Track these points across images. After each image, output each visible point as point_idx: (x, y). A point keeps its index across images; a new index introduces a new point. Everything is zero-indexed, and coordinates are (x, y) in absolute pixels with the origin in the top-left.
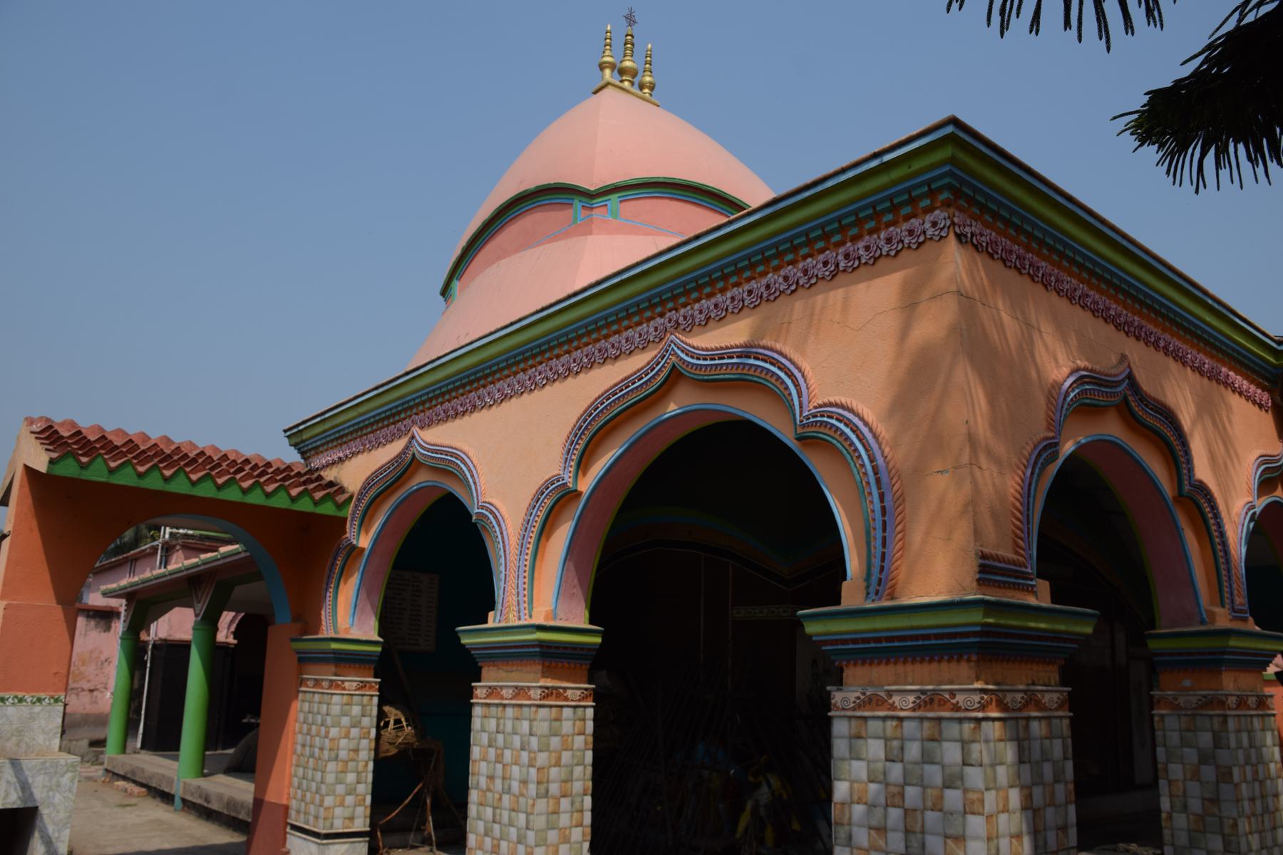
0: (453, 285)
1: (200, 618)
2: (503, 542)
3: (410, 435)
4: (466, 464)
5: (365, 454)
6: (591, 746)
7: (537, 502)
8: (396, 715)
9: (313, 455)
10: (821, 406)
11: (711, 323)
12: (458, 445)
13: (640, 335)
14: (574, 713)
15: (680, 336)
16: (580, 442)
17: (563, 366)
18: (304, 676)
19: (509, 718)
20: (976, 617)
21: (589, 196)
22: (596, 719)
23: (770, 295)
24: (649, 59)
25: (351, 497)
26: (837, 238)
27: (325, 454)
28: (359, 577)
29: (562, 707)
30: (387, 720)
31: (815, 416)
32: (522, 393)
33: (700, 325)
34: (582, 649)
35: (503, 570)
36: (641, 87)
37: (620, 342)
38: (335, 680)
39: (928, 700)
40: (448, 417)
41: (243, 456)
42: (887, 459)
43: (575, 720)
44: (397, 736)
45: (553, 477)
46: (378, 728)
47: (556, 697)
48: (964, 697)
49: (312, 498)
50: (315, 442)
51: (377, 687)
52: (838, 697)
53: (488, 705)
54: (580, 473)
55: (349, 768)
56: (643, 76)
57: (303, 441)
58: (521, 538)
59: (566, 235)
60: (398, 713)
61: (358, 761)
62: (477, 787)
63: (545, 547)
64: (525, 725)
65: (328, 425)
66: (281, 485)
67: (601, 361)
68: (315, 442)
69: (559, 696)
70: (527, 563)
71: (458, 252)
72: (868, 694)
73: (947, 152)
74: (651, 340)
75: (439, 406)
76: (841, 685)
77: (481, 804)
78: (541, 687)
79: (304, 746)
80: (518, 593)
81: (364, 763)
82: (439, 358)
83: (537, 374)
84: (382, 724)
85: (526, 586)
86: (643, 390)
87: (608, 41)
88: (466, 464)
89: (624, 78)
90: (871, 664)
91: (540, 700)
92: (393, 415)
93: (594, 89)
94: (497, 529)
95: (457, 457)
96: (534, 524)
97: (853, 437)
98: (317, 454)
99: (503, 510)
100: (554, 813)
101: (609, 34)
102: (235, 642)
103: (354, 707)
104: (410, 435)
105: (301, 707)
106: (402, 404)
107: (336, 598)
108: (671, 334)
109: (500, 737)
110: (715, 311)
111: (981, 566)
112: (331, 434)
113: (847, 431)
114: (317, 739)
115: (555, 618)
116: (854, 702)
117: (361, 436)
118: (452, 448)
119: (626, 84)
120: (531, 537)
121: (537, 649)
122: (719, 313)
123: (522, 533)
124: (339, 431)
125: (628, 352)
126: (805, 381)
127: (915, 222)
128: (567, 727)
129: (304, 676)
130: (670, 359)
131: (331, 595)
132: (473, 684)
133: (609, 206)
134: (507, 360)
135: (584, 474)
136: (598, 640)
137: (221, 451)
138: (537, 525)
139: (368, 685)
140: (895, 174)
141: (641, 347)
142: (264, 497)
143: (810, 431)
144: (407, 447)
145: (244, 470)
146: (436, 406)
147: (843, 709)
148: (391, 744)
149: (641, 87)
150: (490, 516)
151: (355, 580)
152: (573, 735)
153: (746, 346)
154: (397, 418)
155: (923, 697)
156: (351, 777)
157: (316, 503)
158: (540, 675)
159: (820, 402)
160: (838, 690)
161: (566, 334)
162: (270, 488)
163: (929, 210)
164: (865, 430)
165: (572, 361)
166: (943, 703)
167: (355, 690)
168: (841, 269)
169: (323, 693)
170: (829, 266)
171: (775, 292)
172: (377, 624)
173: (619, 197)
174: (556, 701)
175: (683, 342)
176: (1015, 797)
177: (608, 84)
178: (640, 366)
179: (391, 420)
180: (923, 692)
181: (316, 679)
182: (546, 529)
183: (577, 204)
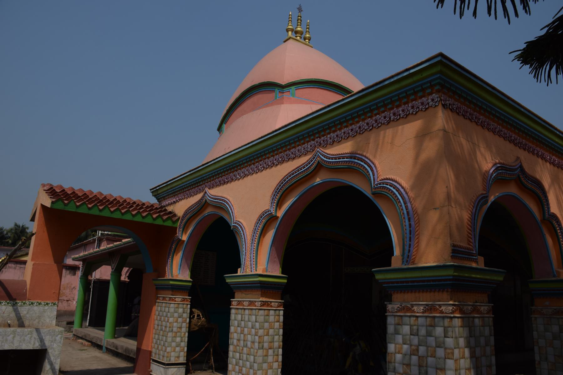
0: (223, 126)
1: (114, 270)
2: (244, 238)
4: (228, 204)
5: (185, 200)
6: (282, 327)
7: (259, 221)
8: (198, 313)
9: (163, 200)
10: (383, 180)
11: (335, 143)
12: (225, 196)
13: (304, 149)
14: (275, 313)
15: (322, 149)
16: (278, 195)
17: (270, 162)
18: (158, 295)
22: (284, 315)
23: (361, 131)
24: (308, 27)
25: (179, 218)
26: (390, 106)
28: (182, 253)
29: (269, 310)
30: (194, 315)
31: (380, 184)
32: (253, 174)
33: (330, 144)
34: (268, 284)
35: (244, 251)
36: (305, 39)
37: (295, 151)
38: (172, 297)
39: (430, 309)
40: (221, 184)
41: (133, 200)
42: (412, 203)
43: (275, 316)
44: (198, 322)
45: (266, 210)
46: (190, 318)
47: (267, 306)
48: (445, 307)
49: (162, 219)
50: (164, 194)
51: (190, 300)
52: (389, 307)
53: (237, 309)
56: (306, 34)
57: (158, 194)
59: (272, 104)
60: (199, 312)
61: (181, 333)
64: (253, 318)
65: (169, 187)
66: (149, 213)
67: (287, 160)
68: (164, 194)
69: (268, 305)
70: (255, 247)
71: (225, 112)
72: (403, 305)
76: (391, 301)
77: (163, 336)
78: (260, 301)
79: (158, 325)
81: (184, 333)
82: (217, 158)
83: (259, 165)
84: (192, 317)
85: (254, 257)
87: (290, 19)
88: (228, 204)
89: (297, 35)
90: (404, 293)
92: (197, 183)
93: (284, 40)
94: (242, 232)
95: (225, 201)
96: (258, 230)
97: (397, 193)
98: (164, 200)
99: (245, 224)
100: (174, 337)
102: (129, 280)
103: (180, 309)
106: (201, 178)
108: (318, 148)
109: (243, 323)
111: (453, 250)
112: (171, 191)
114: (164, 322)
115: (267, 271)
116: (397, 309)
117: (183, 192)
118: (223, 197)
119: (298, 38)
120: (256, 236)
121: (259, 285)
122: (338, 139)
124: (174, 190)
125: (299, 156)
126: (376, 169)
128: (272, 318)
129: (158, 295)
131: (170, 260)
132: (231, 300)
133: (291, 91)
134: (246, 159)
135: (280, 209)
137: (123, 198)
138: (259, 231)
139: (186, 300)
140: (415, 78)
141: (304, 154)
142: (141, 218)
143: (378, 191)
144: (203, 197)
146: (216, 179)
147: (392, 312)
149: (305, 39)
150: (239, 227)
151: (180, 254)
153: (352, 154)
155: (427, 307)
156: (178, 339)
157: (164, 221)
158: (260, 296)
159: (383, 178)
160: (390, 304)
161: (272, 148)
162: (144, 214)
163: (431, 94)
164: (402, 190)
165: (274, 160)
167: (180, 302)
168: (392, 120)
169: (166, 303)
170: (386, 119)
171: (363, 130)
172: (190, 273)
173: (295, 88)
174: (267, 307)
175: (323, 152)
176: (467, 352)
177: (290, 38)
178: (304, 162)
179: (196, 185)
181: (163, 297)
182: (263, 233)
183: (277, 91)
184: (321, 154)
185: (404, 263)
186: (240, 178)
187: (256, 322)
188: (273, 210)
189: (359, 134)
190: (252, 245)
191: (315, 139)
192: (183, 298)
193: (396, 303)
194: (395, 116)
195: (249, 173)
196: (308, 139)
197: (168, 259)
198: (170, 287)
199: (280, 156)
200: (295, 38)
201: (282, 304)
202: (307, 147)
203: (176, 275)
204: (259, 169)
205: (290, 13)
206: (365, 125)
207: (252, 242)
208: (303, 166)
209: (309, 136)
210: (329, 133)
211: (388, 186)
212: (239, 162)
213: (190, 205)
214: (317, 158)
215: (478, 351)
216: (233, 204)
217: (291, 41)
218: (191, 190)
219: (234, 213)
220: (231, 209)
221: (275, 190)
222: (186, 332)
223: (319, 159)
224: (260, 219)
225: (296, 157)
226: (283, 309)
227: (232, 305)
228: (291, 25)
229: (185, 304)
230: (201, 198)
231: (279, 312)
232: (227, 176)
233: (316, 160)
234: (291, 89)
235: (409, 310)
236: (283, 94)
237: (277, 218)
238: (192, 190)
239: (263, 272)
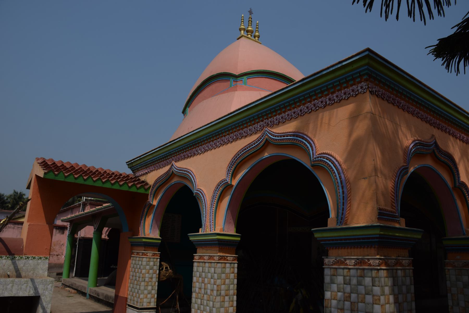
0: (186, 109)
1: (96, 230)
2: (205, 203)
3: (171, 164)
4: (191, 175)
5: (155, 171)
6: (236, 278)
7: (217, 189)
8: (166, 265)
9: (137, 171)
10: (320, 154)
11: (280, 124)
12: (189, 168)
14: (230, 265)
15: (269, 129)
16: (233, 167)
18: (133, 251)
19: (207, 267)
20: (377, 232)
21: (236, 77)
23: (302, 113)
25: (150, 186)
26: (326, 93)
27: (141, 171)
29: (226, 263)
30: (163, 267)
31: (318, 158)
32: (212, 149)
33: (276, 124)
34: (227, 242)
36: (255, 37)
37: (247, 131)
38: (144, 253)
39: (360, 262)
41: (112, 171)
42: (344, 174)
44: (166, 273)
45: (223, 180)
46: (160, 270)
48: (373, 261)
49: (136, 187)
50: (138, 166)
51: (159, 255)
52: (326, 261)
53: (199, 262)
54: (233, 178)
55: (149, 285)
56: (255, 33)
57: (133, 166)
58: (211, 202)
60: (167, 265)
62: (195, 292)
63: (220, 205)
65: (142, 161)
66: (125, 182)
67: (240, 138)
68: (138, 166)
69: (225, 259)
70: (214, 211)
71: (188, 97)
73: (366, 61)
74: (259, 130)
75: (182, 154)
78: (218, 256)
79: (133, 276)
80: (210, 221)
81: (154, 283)
82: (182, 136)
83: (217, 142)
86: (249, 152)
88: (191, 175)
89: (248, 34)
91: (218, 260)
92: (165, 157)
93: (237, 38)
94: (203, 198)
95: (188, 172)
96: (216, 197)
97: (332, 165)
98: (138, 171)
99: (205, 191)
101: (243, 18)
102: (108, 238)
103: (151, 262)
104: (171, 164)
105: (132, 262)
106: (168, 153)
107: (145, 223)
108: (266, 128)
110: (282, 119)
111: (379, 213)
113: (330, 163)
114: (138, 274)
115: (223, 231)
116: (332, 262)
117: (154, 165)
119: (249, 36)
120: (215, 201)
121: (217, 242)
122: (283, 120)
123: (212, 200)
124: (146, 163)
125: (250, 134)
127: (354, 87)
128: (228, 270)
129: (133, 251)
130: (265, 137)
132: (194, 255)
133: (243, 80)
135: (234, 179)
136: (239, 239)
137: (104, 170)
138: (217, 197)
139: (156, 254)
140: (347, 69)
141: (255, 132)
143: (316, 163)
144: (170, 169)
145: (112, 177)
146: (181, 154)
147: (328, 265)
148: (164, 276)
149: (255, 37)
150: (200, 194)
151: (151, 217)
152: (230, 273)
154: (167, 158)
155: (357, 261)
156: (150, 288)
157: (138, 189)
158: (218, 251)
160: (327, 258)
162: (121, 183)
163: (360, 82)
164: (336, 163)
165: (230, 137)
166: (365, 263)
167: (151, 256)
168: (328, 104)
169: (140, 257)
170: (323, 103)
171: (303, 113)
173: (247, 77)
174: (224, 261)
175: (270, 131)
176: (391, 298)
177: (242, 36)
178: (254, 139)
179: (165, 159)
180: (358, 259)
181: (137, 252)
182: (220, 199)
183: (232, 80)
184: (268, 133)
185: (338, 223)
186: (201, 153)
187: (215, 273)
188: (229, 180)
189: (300, 116)
190: (211, 209)
191: (264, 120)
192: (154, 253)
193: (331, 257)
194: (331, 101)
195: (209, 149)
196: (257, 121)
197: (141, 220)
198: (143, 244)
199: (234, 135)
200: (247, 36)
201: (236, 259)
202: (257, 127)
203: (148, 234)
204: (217, 146)
205: (243, 16)
206: (306, 108)
207: (211, 206)
208: (254, 142)
209: (259, 118)
210: (275, 115)
211: (325, 160)
212: (200, 140)
213: (160, 175)
214: (266, 136)
215: (400, 297)
216: (195, 175)
217: (243, 38)
218: (160, 163)
219: (196, 182)
220: (194, 179)
221: (230, 162)
222: (156, 282)
223: (267, 137)
224: (218, 187)
225: (248, 136)
226: (238, 262)
227: (194, 259)
228: (243, 25)
229: (209, 262)
230: (169, 170)
231: (234, 265)
232: (190, 151)
233: (265, 137)
234: (243, 78)
235: (342, 263)
236: (237, 82)
237: (232, 186)
238: (162, 163)
239: (220, 232)
